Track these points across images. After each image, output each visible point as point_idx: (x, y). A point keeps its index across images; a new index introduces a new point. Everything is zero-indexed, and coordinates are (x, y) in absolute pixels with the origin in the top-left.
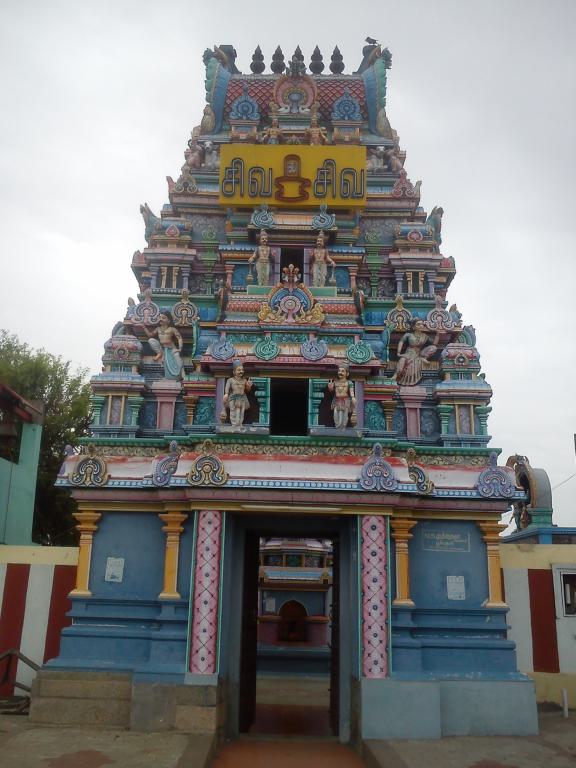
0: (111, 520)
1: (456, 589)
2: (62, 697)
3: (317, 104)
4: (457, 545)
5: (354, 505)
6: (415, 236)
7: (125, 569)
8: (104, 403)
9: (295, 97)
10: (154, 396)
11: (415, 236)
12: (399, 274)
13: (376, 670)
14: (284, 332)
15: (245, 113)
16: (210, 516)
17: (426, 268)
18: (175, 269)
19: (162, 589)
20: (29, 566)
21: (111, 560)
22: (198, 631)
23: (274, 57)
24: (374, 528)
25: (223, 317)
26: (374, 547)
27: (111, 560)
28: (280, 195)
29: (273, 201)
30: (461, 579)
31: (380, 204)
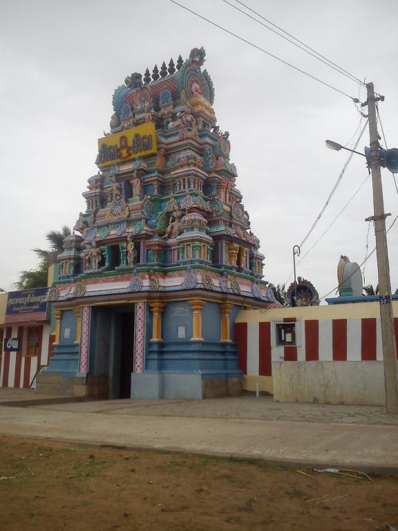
0: (66, 313)
1: (181, 333)
2: (44, 383)
3: (152, 99)
4: (183, 312)
5: (132, 299)
6: (183, 160)
7: (70, 333)
8: (184, 248)
9: (143, 99)
10: (170, 246)
11: (183, 160)
12: (177, 180)
13: (139, 369)
14: (115, 223)
15: (126, 113)
16: (86, 309)
17: (188, 175)
18: (186, 178)
19: (75, 340)
20: (317, 321)
21: (66, 330)
22: (82, 356)
23: (153, 71)
24: (140, 308)
25: (95, 221)
26: (140, 316)
27: (66, 330)
28: (120, 156)
29: (119, 160)
30: (184, 328)
31: (175, 145)
